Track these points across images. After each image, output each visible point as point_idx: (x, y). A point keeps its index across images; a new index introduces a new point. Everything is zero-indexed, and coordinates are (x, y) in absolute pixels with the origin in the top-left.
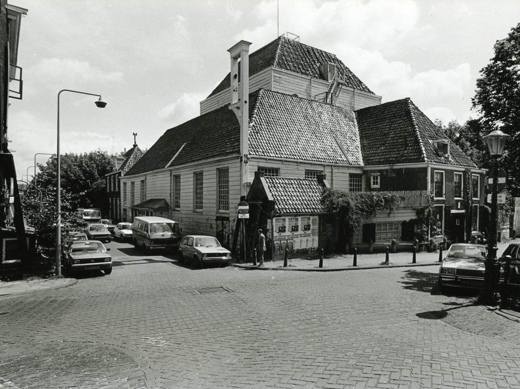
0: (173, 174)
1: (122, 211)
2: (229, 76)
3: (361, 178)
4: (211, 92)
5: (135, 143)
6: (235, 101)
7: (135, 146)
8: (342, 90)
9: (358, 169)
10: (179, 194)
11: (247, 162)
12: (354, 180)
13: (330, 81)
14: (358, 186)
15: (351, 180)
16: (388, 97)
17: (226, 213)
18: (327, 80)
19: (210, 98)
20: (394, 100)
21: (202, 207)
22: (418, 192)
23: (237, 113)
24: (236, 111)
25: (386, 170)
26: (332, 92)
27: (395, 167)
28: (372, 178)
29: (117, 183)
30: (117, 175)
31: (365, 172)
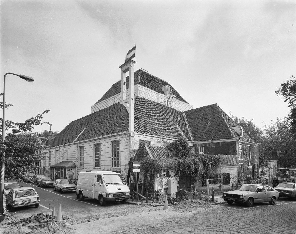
0: (78, 146)
4: (97, 101)
5: (50, 130)
6: (124, 97)
13: (167, 95)
17: (118, 169)
18: (166, 95)
19: (95, 105)
20: (208, 105)
21: (83, 166)
22: (232, 156)
23: (127, 106)
25: (209, 144)
27: (214, 142)
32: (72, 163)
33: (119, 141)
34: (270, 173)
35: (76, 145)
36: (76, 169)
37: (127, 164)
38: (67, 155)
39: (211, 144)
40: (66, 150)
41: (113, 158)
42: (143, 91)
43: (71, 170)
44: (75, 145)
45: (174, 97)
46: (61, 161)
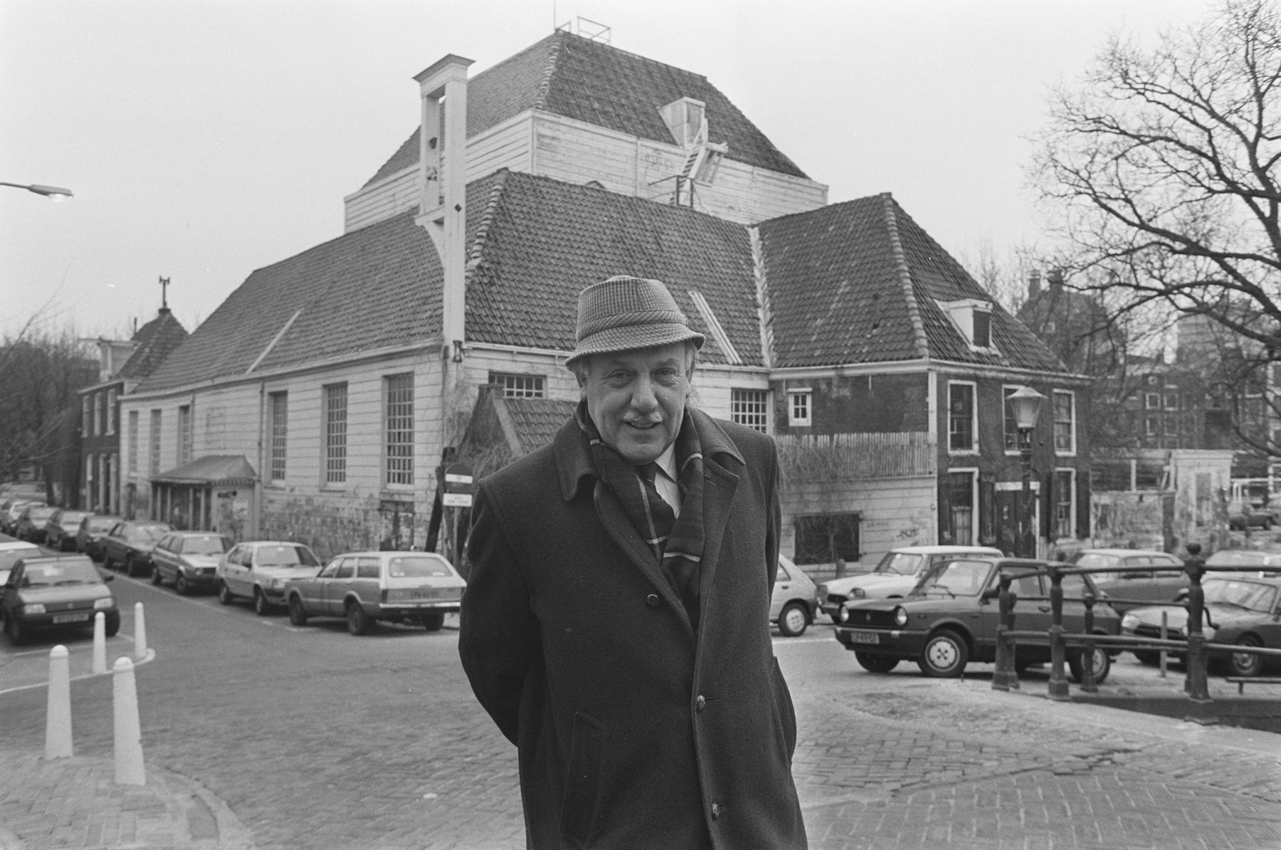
0: (267, 390)
1: (123, 491)
2: (416, 136)
3: (764, 399)
4: (374, 172)
7: (164, 311)
8: (720, 169)
9: (755, 377)
10: (283, 442)
11: (460, 361)
12: (744, 406)
14: (757, 422)
15: (737, 406)
16: (844, 188)
19: (369, 188)
20: (853, 198)
21: (342, 478)
24: (433, 230)
25: (829, 381)
26: (692, 175)
27: (847, 373)
28: (791, 400)
29: (110, 413)
30: (112, 391)
31: (775, 386)
32: (241, 463)
33: (409, 376)
34: (1172, 514)
35: (259, 386)
36: (253, 494)
37: (433, 472)
38: (222, 428)
39: (835, 382)
40: (220, 405)
41: (389, 447)
42: (561, 136)
43: (235, 494)
44: (253, 386)
45: (720, 154)
46: (198, 455)
